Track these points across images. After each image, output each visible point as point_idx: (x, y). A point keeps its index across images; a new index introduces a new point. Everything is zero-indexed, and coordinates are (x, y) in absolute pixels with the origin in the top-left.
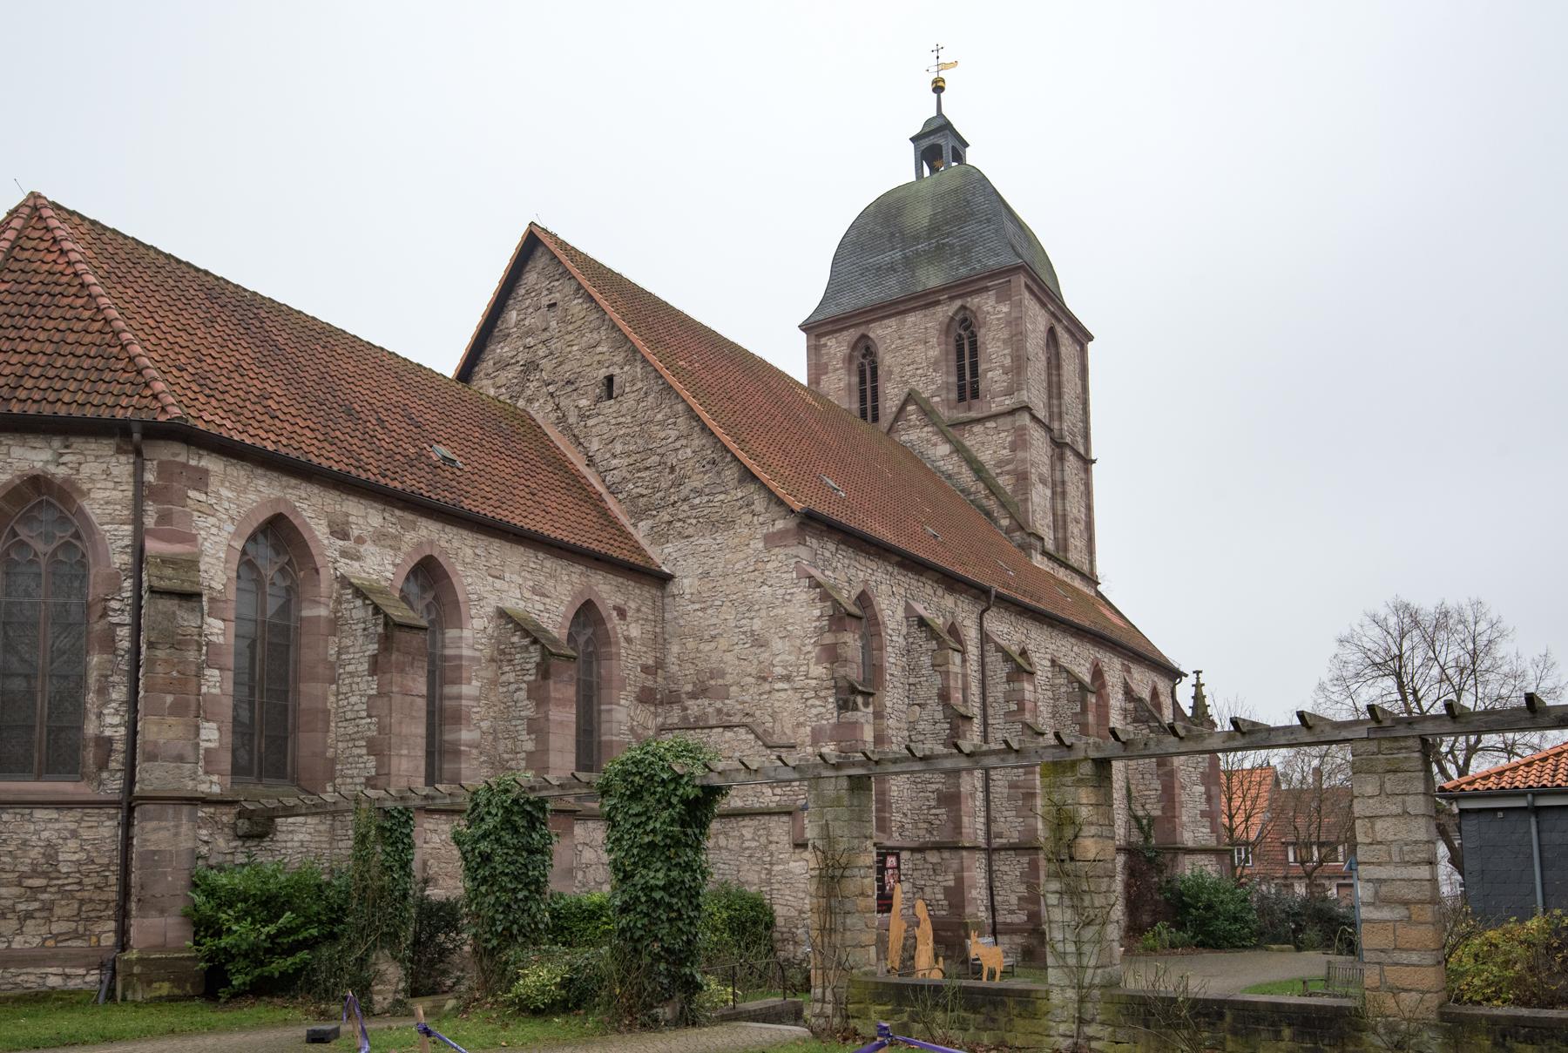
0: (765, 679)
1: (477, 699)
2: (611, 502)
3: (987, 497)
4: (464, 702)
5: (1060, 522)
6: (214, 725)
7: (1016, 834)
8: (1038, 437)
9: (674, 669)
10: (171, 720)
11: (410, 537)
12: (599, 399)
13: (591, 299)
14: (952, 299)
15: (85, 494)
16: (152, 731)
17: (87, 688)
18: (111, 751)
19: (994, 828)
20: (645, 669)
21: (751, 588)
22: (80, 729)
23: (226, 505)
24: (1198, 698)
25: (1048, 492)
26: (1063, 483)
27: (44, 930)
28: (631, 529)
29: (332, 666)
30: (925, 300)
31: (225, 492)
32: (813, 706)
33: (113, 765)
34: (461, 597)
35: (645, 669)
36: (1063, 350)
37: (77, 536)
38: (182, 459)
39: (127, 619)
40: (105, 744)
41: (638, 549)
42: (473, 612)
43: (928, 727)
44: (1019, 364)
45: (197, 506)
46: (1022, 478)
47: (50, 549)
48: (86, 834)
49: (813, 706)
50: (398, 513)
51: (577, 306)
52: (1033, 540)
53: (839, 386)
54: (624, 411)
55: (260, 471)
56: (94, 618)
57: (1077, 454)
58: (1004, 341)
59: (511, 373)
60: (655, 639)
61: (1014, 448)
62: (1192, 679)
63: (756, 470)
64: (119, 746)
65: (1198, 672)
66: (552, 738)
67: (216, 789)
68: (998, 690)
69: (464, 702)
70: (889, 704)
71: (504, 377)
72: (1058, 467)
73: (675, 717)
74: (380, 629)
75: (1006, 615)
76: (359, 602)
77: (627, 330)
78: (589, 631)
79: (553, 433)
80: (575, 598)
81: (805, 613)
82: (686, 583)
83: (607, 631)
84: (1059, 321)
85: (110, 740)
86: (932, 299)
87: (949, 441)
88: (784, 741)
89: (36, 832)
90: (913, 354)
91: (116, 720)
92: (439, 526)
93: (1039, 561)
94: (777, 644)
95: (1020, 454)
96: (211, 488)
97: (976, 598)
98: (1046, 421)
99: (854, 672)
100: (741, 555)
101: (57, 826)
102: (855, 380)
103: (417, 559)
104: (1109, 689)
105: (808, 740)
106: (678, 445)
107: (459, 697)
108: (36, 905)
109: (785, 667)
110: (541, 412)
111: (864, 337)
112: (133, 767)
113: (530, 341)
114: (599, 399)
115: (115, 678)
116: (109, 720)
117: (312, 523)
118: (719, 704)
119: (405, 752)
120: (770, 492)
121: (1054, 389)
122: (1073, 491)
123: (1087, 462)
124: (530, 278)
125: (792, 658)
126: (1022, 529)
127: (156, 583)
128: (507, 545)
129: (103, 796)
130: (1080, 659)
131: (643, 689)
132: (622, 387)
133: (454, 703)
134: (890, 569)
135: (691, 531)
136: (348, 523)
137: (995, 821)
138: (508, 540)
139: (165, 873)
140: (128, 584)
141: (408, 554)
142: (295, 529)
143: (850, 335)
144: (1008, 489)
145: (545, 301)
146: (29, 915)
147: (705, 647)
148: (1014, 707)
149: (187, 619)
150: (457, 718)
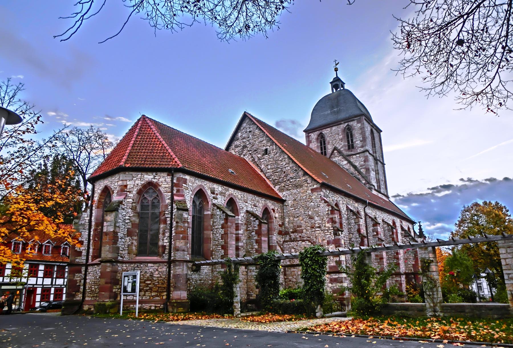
0: (313, 228)
1: (242, 234)
8: (371, 158)
10: (182, 241)
12: (263, 155)
13: (260, 129)
14: (345, 123)
18: (165, 249)
20: (280, 225)
21: (308, 203)
24: (420, 229)
26: (378, 170)
28: (274, 188)
29: (212, 226)
30: (337, 123)
31: (190, 184)
33: (166, 253)
35: (280, 225)
36: (375, 135)
37: (157, 196)
38: (182, 176)
39: (169, 216)
40: (164, 247)
41: (277, 194)
44: (364, 140)
46: (368, 170)
47: (151, 199)
51: (257, 132)
52: (372, 187)
53: (314, 146)
56: (162, 216)
58: (360, 134)
61: (365, 161)
62: (418, 224)
64: (167, 248)
65: (419, 222)
68: (371, 229)
71: (237, 150)
76: (218, 210)
77: (271, 137)
79: (251, 164)
81: (324, 209)
85: (165, 246)
86: (339, 123)
87: (346, 160)
89: (149, 269)
90: (335, 137)
91: (167, 241)
93: (374, 192)
94: (316, 218)
95: (367, 163)
99: (338, 225)
102: (319, 144)
105: (326, 244)
108: (148, 288)
110: (248, 158)
111: (321, 133)
113: (244, 140)
114: (263, 155)
115: (166, 231)
116: (165, 241)
118: (300, 235)
121: (374, 145)
122: (381, 172)
123: (383, 164)
124: (244, 125)
125: (320, 222)
129: (164, 260)
130: (389, 219)
131: (280, 231)
132: (270, 152)
135: (290, 188)
140: (170, 207)
143: (317, 133)
144: (364, 173)
145: (248, 130)
146: (147, 291)
147: (296, 219)
148: (375, 234)
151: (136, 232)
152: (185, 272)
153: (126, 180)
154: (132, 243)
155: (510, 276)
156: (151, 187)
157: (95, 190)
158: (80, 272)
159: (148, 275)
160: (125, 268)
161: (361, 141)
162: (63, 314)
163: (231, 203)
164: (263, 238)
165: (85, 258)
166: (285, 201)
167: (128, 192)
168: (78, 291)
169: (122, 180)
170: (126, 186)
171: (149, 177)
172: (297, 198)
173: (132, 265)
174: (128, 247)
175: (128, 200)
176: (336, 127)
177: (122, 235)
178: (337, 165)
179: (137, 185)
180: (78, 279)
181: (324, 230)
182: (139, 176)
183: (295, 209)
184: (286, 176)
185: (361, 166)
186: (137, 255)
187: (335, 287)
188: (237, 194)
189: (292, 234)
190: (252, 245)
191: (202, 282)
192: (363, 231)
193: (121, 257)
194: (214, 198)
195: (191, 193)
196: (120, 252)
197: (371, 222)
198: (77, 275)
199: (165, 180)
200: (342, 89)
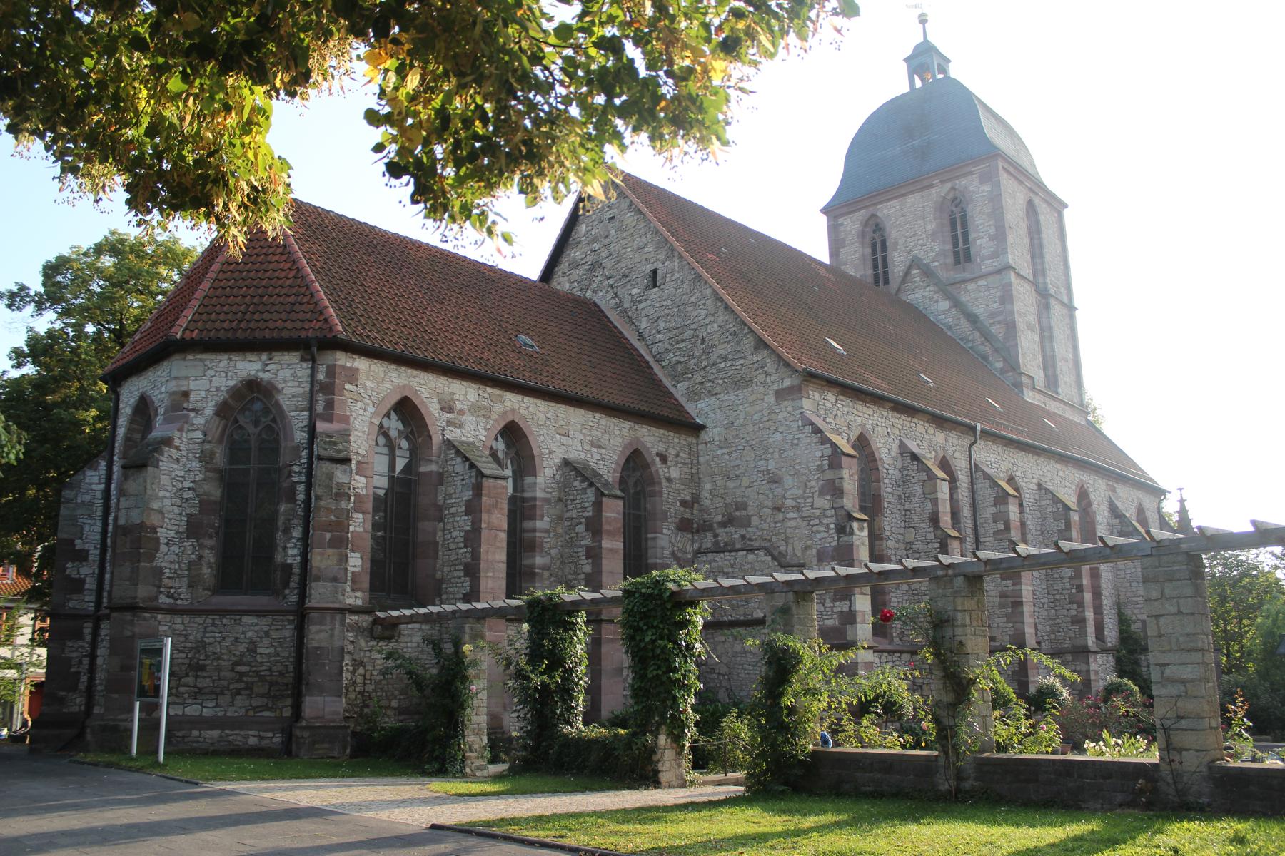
1: (547, 531)
2: (657, 370)
4: (538, 534)
6: (358, 555)
9: (707, 502)
10: (330, 551)
12: (647, 288)
13: (639, 212)
14: (943, 182)
15: (278, 391)
17: (277, 529)
18: (291, 574)
20: (684, 503)
23: (370, 393)
24: (1183, 512)
25: (1037, 338)
27: (247, 703)
28: (672, 390)
32: (818, 532)
33: (293, 585)
34: (536, 452)
36: (1042, 218)
37: (274, 420)
39: (303, 478)
42: (545, 463)
43: (922, 547)
45: (351, 395)
46: (1011, 327)
48: (274, 635)
49: (818, 532)
50: (489, 390)
51: (630, 219)
54: (665, 296)
55: (393, 367)
57: (1062, 303)
59: (580, 272)
60: (691, 480)
63: (768, 339)
64: (296, 570)
65: (1181, 489)
66: (604, 562)
67: (359, 602)
69: (538, 534)
70: (887, 528)
74: (473, 480)
75: (994, 447)
78: (638, 474)
79: (613, 316)
80: (625, 448)
82: (715, 433)
83: (651, 474)
84: (1037, 194)
85: (291, 566)
86: (1022, 178)
87: (948, 296)
88: (795, 561)
89: (243, 633)
91: (295, 552)
94: (788, 481)
95: (1008, 307)
96: (360, 382)
98: (1031, 278)
100: (758, 408)
101: (257, 628)
102: (868, 250)
103: (502, 424)
104: (1095, 507)
106: (707, 321)
107: (534, 530)
108: (243, 685)
109: (794, 500)
110: (603, 299)
111: (873, 216)
113: (596, 246)
114: (647, 288)
115: (295, 521)
117: (427, 401)
118: (743, 532)
119: (490, 574)
120: (779, 357)
123: (1071, 309)
127: (322, 453)
128: (571, 409)
131: (682, 520)
133: (530, 535)
134: (885, 413)
135: (718, 389)
138: (572, 405)
139: (324, 665)
140: (304, 453)
141: (496, 421)
142: (415, 407)
143: (861, 215)
144: (1000, 336)
147: (731, 484)
148: (1001, 527)
149: (340, 475)
150: (532, 546)
152: (337, 644)
153: (187, 378)
154: (200, 557)
156: (254, 394)
157: (121, 405)
158: (79, 635)
159: (242, 648)
160: (181, 627)
161: (991, 239)
163: (513, 433)
164: (606, 544)
165: (93, 598)
166: (702, 427)
167: (192, 410)
168: (74, 688)
169: (176, 378)
170: (186, 395)
171: (248, 366)
173: (199, 620)
174: (189, 569)
175: (191, 435)
176: (918, 195)
177: (172, 534)
178: (914, 313)
179: (218, 389)
180: (74, 655)
181: (809, 518)
182: (222, 364)
183: (730, 453)
184: (707, 352)
185: (993, 315)
188: (532, 411)
189: (720, 531)
190: (577, 564)
192: (946, 520)
193: (169, 596)
194: (449, 423)
196: (166, 581)
197: (989, 491)
198: (70, 644)
199: (294, 375)
200: (940, 76)
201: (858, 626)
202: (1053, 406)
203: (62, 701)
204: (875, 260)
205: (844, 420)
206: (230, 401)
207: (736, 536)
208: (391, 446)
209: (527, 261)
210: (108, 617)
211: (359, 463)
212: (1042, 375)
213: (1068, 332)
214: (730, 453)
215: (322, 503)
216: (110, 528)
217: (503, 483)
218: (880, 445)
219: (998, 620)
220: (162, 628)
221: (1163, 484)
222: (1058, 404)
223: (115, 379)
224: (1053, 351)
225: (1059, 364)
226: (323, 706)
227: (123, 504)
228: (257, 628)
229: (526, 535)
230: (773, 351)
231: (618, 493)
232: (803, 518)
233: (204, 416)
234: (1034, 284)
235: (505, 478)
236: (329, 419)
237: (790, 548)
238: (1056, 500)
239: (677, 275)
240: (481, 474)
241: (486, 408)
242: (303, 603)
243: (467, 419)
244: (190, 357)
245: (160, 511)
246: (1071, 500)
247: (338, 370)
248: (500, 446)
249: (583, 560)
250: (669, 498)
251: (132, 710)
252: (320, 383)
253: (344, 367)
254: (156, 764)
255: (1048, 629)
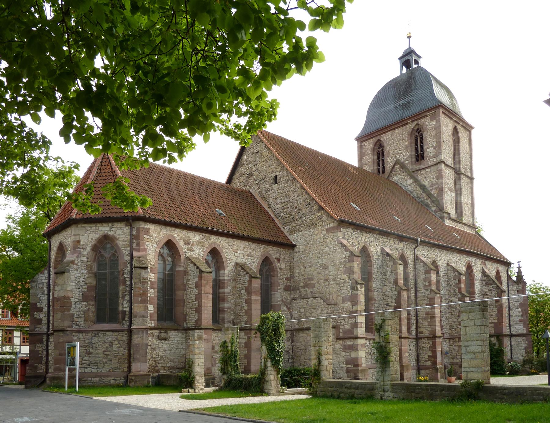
0: (327, 280)
1: (230, 293)
2: (276, 221)
3: (427, 199)
5: (458, 206)
6: (152, 306)
7: (428, 332)
10: (141, 305)
11: (208, 242)
12: (272, 184)
13: (269, 149)
14: (413, 121)
15: (117, 239)
16: (135, 309)
19: (420, 330)
20: (287, 279)
22: (117, 308)
24: (519, 272)
25: (453, 194)
28: (283, 230)
31: (154, 235)
32: (343, 289)
33: (126, 319)
34: (224, 260)
36: (460, 135)
37: (116, 252)
39: (129, 275)
40: (124, 312)
43: (390, 294)
46: (441, 191)
47: (109, 256)
49: (343, 289)
50: (204, 234)
51: (265, 152)
52: (445, 215)
55: (164, 227)
56: (120, 276)
57: (467, 177)
58: (434, 136)
59: (244, 178)
60: (290, 269)
63: (323, 205)
64: (127, 313)
65: (519, 262)
66: (252, 305)
67: (153, 325)
68: (422, 277)
72: (458, 183)
73: (297, 295)
74: (198, 273)
75: (426, 248)
78: (268, 267)
79: (258, 198)
82: (300, 248)
84: (459, 123)
85: (125, 311)
86: (405, 122)
88: (333, 302)
89: (107, 339)
90: (398, 145)
91: (127, 306)
92: (217, 237)
93: (448, 223)
94: (331, 268)
95: (440, 181)
97: (413, 243)
98: (453, 166)
100: (319, 237)
101: (112, 337)
102: (376, 157)
103: (210, 249)
104: (475, 273)
105: (341, 302)
106: (298, 198)
107: (224, 293)
108: (108, 359)
109: (333, 276)
110: (253, 190)
111: (379, 140)
112: (131, 319)
113: (250, 166)
114: (272, 184)
115: (126, 293)
116: (125, 306)
118: (311, 290)
121: (456, 151)
123: (471, 179)
126: (441, 210)
127: (136, 265)
128: (239, 241)
129: (123, 328)
130: (460, 263)
131: (286, 286)
132: (280, 180)
134: (375, 236)
135: (302, 229)
136: (190, 240)
137: (420, 327)
140: (129, 265)
143: (374, 140)
144: (435, 195)
145: (255, 151)
147: (307, 270)
148: (427, 284)
149: (143, 273)
150: (223, 300)
151: (93, 297)
152: (145, 342)
154: (89, 309)
155: (468, 349)
157: (52, 247)
158: (41, 342)
160: (82, 337)
162: (26, 388)
164: (253, 298)
165: (46, 326)
166: (295, 246)
167: (82, 248)
168: (41, 363)
169: (74, 235)
170: (79, 242)
171: (104, 229)
172: (309, 241)
173: (90, 334)
174: (84, 314)
175: (82, 259)
176: (400, 129)
177: (76, 300)
178: (397, 187)
179: (92, 239)
180: (40, 349)
182: (94, 228)
185: (432, 185)
186: (95, 323)
187: (349, 357)
188: (222, 242)
189: (302, 290)
190: (241, 306)
191: (172, 351)
192: (401, 282)
193: (77, 325)
194: (188, 250)
195: (155, 245)
196: (75, 319)
198: (38, 345)
201: (359, 329)
202: (459, 227)
203: (36, 368)
204: (379, 162)
205: (355, 240)
206: (98, 245)
207: (309, 292)
208: (164, 260)
209: (220, 176)
210: (52, 334)
211: (151, 268)
212: (454, 212)
213: (470, 190)
214: (306, 257)
215: (137, 286)
216: (51, 298)
217: (211, 274)
218: (372, 250)
219: (424, 324)
220: (74, 338)
221: (510, 260)
222: (461, 225)
223: (49, 235)
224: (461, 200)
225: (463, 206)
226: (140, 368)
227: (56, 288)
228: (112, 337)
229: (221, 295)
230: (326, 211)
231: (258, 276)
232: (337, 284)
233: (87, 251)
234: (454, 168)
235: (211, 272)
236: (139, 250)
237: (331, 296)
238: (455, 270)
239: (285, 178)
240: (201, 272)
241: (203, 243)
242: (131, 326)
243: (196, 248)
244: (79, 226)
245: (71, 291)
246: (463, 269)
247: (141, 230)
248: (210, 258)
249: (244, 305)
250: (281, 277)
251: (65, 371)
252: (134, 235)
253: (143, 228)
254: (76, 391)
255: (448, 327)
